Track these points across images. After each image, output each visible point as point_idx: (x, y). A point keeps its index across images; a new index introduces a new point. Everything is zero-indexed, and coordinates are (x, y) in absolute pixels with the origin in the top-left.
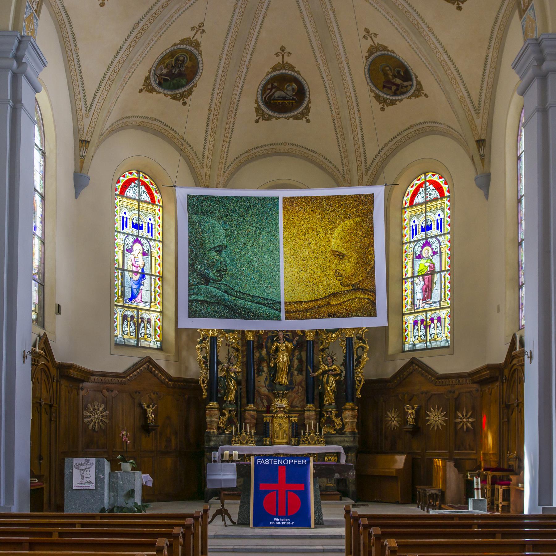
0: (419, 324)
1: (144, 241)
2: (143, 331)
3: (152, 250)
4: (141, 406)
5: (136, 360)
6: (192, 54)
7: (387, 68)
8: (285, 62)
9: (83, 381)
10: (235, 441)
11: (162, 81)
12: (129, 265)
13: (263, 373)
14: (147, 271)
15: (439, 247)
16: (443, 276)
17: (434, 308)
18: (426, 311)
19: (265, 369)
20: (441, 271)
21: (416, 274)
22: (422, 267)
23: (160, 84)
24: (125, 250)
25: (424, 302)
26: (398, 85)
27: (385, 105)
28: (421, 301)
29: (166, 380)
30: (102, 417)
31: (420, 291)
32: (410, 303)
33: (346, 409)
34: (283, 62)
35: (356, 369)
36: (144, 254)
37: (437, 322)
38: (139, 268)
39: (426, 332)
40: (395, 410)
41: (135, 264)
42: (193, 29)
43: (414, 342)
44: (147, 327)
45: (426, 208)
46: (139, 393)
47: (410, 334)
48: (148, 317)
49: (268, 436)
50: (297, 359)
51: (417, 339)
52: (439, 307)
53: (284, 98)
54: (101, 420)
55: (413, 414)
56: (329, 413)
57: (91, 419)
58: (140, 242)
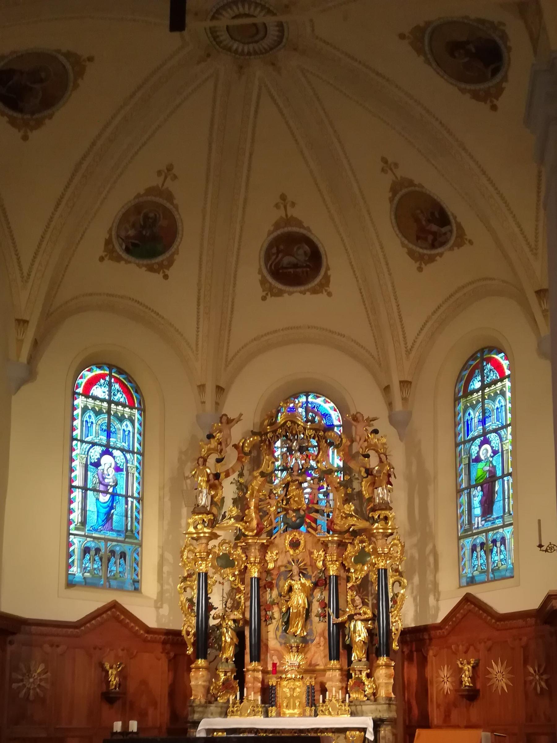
0: (478, 549)
1: (116, 453)
2: (114, 568)
3: (128, 465)
4: (102, 666)
5: (100, 605)
6: (165, 208)
7: (419, 211)
8: (289, 215)
9: (14, 633)
10: (233, 712)
11: (131, 247)
12: (94, 482)
13: (273, 621)
14: (121, 490)
15: (500, 444)
16: (506, 482)
17: (496, 526)
18: (487, 531)
19: (277, 615)
20: (503, 476)
21: (473, 483)
22: (480, 473)
23: (128, 250)
24: (89, 463)
25: (484, 519)
26: (434, 234)
27: (422, 263)
28: (480, 518)
29: (142, 632)
30: (40, 682)
31: (478, 505)
32: (467, 522)
33: (379, 666)
34: (287, 215)
35: (391, 612)
36: (118, 469)
37: (501, 545)
38: (109, 487)
39: (487, 559)
40: (448, 667)
41: (103, 482)
42: (159, 173)
43: (472, 574)
44: (120, 564)
45: (483, 394)
46: (100, 649)
47: (467, 563)
48: (122, 550)
49: (275, 705)
50: (318, 601)
51: (477, 570)
52: (502, 524)
53: (295, 266)
54: (39, 686)
55: (469, 671)
56: (358, 673)
57: (24, 684)
58: (111, 454)
